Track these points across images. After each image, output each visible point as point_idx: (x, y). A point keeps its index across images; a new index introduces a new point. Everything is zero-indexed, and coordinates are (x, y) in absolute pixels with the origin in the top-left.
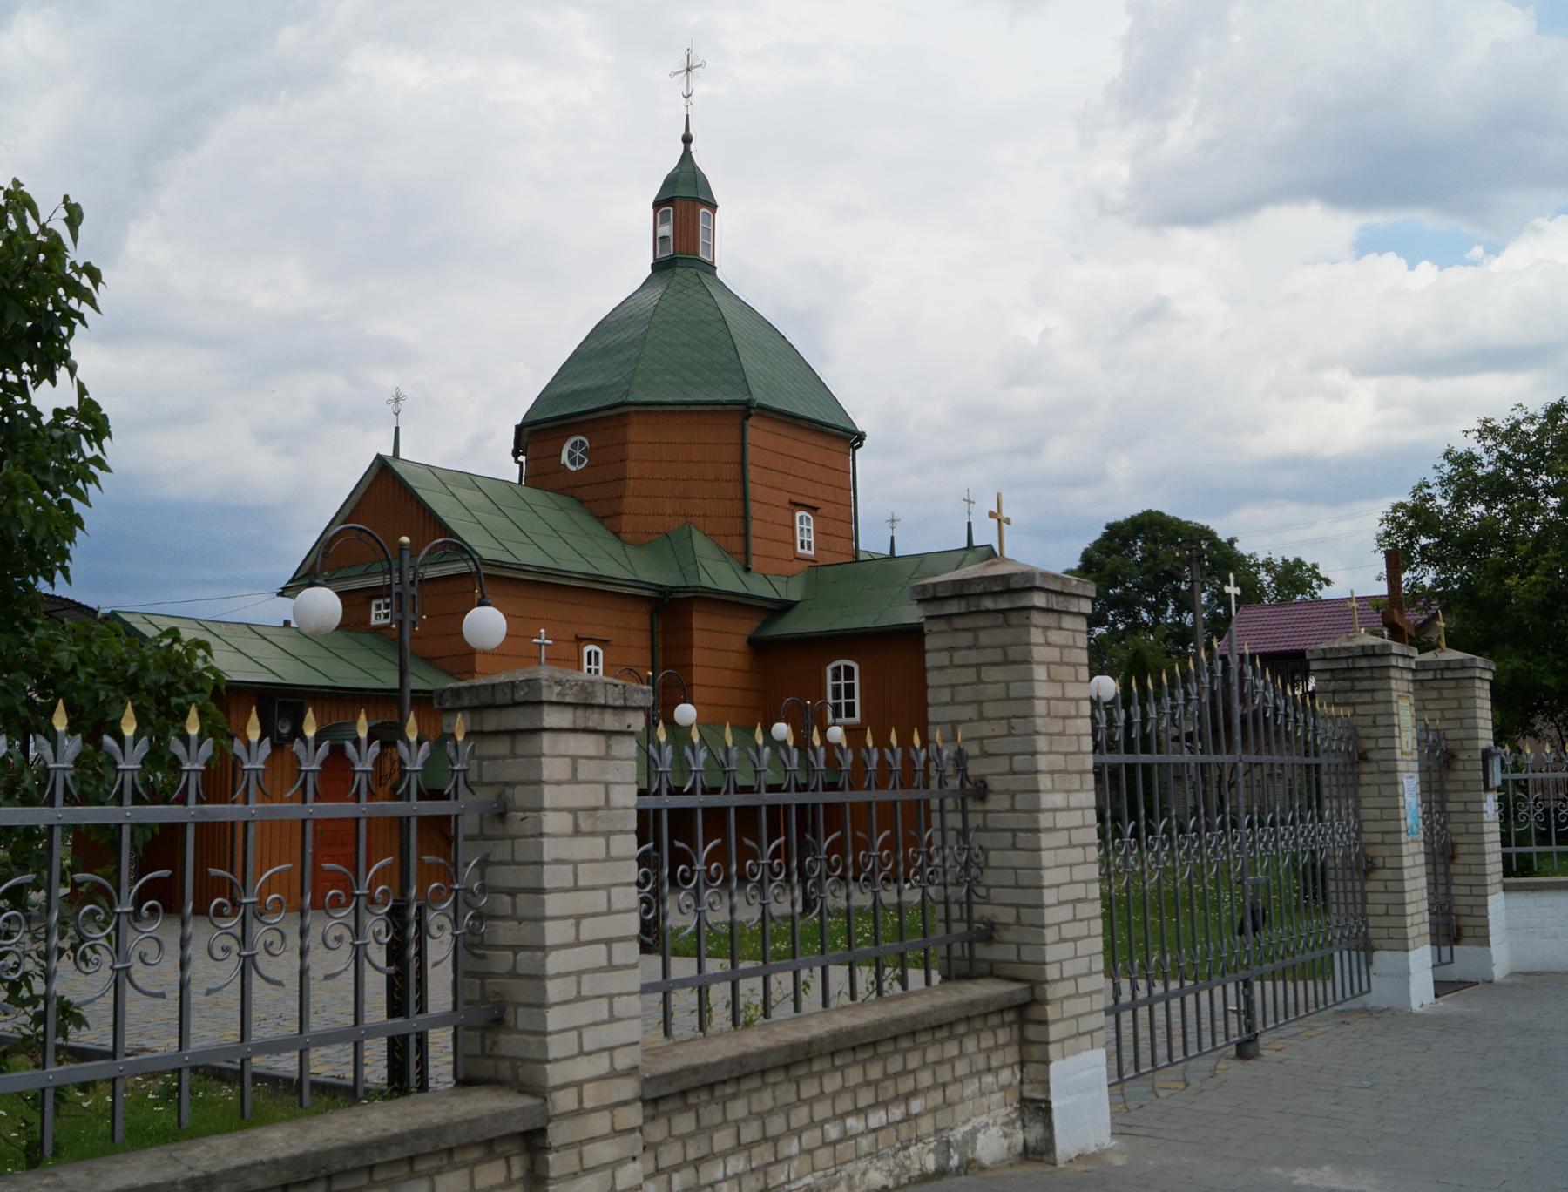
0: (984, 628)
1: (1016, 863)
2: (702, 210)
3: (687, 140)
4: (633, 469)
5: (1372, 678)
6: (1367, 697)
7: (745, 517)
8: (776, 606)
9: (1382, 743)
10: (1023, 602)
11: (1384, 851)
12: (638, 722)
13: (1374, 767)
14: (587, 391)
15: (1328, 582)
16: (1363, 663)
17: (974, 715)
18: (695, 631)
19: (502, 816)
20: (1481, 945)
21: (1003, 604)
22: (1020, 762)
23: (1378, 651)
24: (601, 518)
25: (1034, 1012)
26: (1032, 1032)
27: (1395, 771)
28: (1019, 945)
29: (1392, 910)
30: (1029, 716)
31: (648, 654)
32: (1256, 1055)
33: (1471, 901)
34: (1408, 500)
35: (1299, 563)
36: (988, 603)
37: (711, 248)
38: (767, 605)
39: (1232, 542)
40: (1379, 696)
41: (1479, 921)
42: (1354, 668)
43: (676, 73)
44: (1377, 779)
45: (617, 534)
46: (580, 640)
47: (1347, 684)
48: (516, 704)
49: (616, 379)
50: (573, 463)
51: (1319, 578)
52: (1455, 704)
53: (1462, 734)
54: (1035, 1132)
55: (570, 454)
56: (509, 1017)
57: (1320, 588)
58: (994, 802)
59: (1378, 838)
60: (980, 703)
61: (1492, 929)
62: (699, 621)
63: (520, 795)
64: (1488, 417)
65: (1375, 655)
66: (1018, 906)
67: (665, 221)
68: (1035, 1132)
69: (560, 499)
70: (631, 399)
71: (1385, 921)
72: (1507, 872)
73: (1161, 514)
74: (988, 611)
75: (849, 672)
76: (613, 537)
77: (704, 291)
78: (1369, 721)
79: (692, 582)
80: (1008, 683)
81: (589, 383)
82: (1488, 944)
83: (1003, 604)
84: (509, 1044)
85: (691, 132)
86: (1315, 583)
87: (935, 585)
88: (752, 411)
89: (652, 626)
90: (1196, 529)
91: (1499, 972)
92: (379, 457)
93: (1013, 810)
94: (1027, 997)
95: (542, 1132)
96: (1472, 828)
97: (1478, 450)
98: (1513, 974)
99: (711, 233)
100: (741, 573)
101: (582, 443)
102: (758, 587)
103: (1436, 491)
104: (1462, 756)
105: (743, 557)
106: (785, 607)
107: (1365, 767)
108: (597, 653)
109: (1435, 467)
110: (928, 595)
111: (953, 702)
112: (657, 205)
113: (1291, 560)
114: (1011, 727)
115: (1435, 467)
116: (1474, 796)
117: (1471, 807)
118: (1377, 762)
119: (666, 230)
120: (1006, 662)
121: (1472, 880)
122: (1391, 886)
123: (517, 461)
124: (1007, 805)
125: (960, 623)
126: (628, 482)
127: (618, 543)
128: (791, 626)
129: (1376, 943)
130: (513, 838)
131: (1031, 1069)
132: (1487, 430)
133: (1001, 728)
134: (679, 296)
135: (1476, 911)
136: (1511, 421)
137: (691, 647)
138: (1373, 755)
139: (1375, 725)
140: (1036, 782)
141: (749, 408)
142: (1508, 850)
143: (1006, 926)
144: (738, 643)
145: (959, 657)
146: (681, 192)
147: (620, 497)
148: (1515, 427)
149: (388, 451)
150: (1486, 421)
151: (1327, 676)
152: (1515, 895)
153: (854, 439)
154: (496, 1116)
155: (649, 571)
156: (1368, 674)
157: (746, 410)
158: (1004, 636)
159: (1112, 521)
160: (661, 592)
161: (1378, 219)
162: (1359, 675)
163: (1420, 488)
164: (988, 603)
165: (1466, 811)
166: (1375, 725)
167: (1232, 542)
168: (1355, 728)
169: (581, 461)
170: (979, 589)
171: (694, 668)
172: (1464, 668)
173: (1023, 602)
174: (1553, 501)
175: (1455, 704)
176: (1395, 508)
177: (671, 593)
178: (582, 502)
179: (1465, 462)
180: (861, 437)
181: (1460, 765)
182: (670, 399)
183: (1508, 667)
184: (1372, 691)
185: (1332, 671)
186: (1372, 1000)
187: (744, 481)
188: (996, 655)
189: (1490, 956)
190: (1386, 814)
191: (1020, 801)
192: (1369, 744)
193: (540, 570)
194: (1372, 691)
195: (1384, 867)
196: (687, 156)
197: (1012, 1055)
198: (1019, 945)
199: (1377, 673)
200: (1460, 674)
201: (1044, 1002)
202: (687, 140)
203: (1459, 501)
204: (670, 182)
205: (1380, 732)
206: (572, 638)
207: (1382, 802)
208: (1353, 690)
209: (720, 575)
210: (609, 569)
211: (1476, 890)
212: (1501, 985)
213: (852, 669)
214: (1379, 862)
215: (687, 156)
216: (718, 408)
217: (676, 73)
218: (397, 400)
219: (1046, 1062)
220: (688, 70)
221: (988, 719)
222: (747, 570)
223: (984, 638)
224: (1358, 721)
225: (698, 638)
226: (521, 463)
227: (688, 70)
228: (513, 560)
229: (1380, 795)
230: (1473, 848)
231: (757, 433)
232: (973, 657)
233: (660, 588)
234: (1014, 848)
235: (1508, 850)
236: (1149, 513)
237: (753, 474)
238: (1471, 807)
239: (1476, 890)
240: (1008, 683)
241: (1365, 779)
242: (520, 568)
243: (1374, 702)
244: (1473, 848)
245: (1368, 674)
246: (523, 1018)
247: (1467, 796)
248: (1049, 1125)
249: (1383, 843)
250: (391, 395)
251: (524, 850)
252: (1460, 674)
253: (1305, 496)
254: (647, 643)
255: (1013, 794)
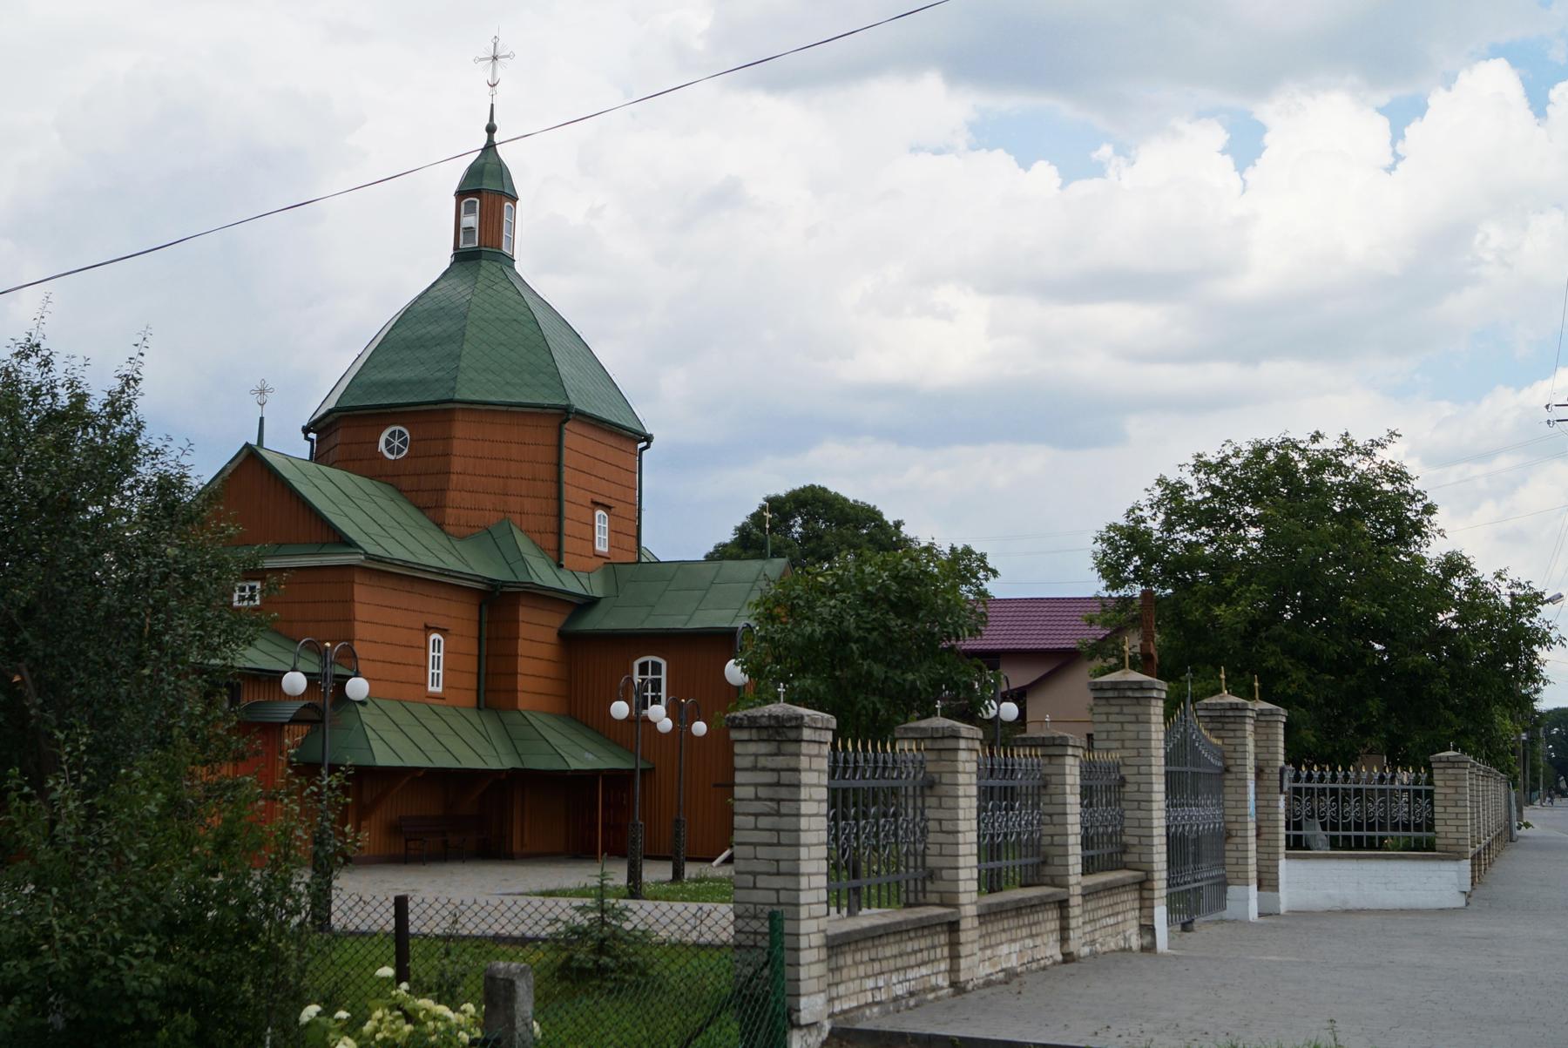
0: (1126, 705)
1: (1139, 816)
2: (507, 204)
3: (491, 129)
4: (457, 464)
5: (1235, 723)
6: (1231, 734)
7: (559, 516)
8: (579, 601)
9: (1239, 762)
10: (1148, 694)
11: (1237, 826)
12: (829, 736)
13: (1232, 776)
14: (408, 382)
15: (995, 573)
16: (1230, 713)
17: (1120, 746)
18: (521, 625)
19: (1045, 787)
20: (1272, 891)
21: (1138, 694)
22: (1143, 769)
23: (1240, 707)
24: (422, 509)
25: (1147, 885)
26: (1146, 894)
27: (1246, 779)
28: (1140, 854)
29: (1240, 861)
30: (1149, 748)
31: (475, 642)
32: (1191, 930)
33: (1268, 863)
34: (1122, 522)
35: (968, 551)
36: (1130, 693)
37: (512, 241)
38: (575, 600)
39: (898, 524)
40: (1239, 734)
41: (1273, 876)
42: (1224, 716)
43: (481, 59)
44: (1236, 783)
45: (440, 525)
46: (428, 629)
47: (1220, 725)
48: (1054, 745)
49: (439, 374)
50: (391, 451)
51: (986, 568)
52: (1265, 737)
53: (1268, 756)
54: (1147, 939)
55: (388, 443)
56: (1050, 861)
57: (987, 579)
58: (1128, 788)
59: (1233, 819)
60: (1123, 740)
61: (1280, 881)
62: (524, 613)
63: (1054, 779)
64: (1201, 453)
65: (1237, 709)
66: (1140, 836)
67: (470, 211)
68: (1147, 939)
69: (383, 487)
70: (457, 397)
71: (1236, 868)
72: (1288, 847)
73: (825, 490)
74: (1129, 697)
75: (657, 668)
76: (436, 528)
77: (512, 288)
78: (1232, 748)
79: (523, 578)
80: (1138, 732)
81: (408, 374)
82: (1277, 891)
83: (1138, 694)
84: (1048, 870)
85: (496, 122)
86: (981, 574)
87: (1102, 682)
88: (571, 416)
89: (480, 616)
90: (863, 509)
91: (1283, 909)
92: (247, 445)
93: (1138, 791)
94: (1145, 878)
95: (1067, 900)
96: (1271, 817)
97: (1191, 481)
98: (1289, 911)
99: (513, 225)
100: (555, 569)
101: (401, 434)
102: (572, 586)
103: (1147, 513)
104: (1268, 770)
105: (554, 554)
106: (589, 603)
107: (1229, 776)
108: (439, 641)
109: (1146, 490)
110: (1098, 687)
111: (1108, 739)
112: (461, 194)
113: (960, 547)
114: (1139, 753)
115: (1146, 490)
116: (1273, 796)
117: (1271, 803)
118: (1236, 773)
119: (471, 221)
120: (1138, 722)
121: (1270, 850)
122: (1240, 847)
123: (307, 438)
124: (1136, 789)
125: (1113, 702)
126: (452, 476)
127: (442, 538)
128: (597, 621)
129: (1229, 881)
130: (1051, 795)
131: (1145, 912)
132: (1201, 465)
133: (1134, 753)
134: (489, 291)
135: (1271, 870)
136: (1222, 455)
137: (517, 638)
138: (1234, 769)
139: (1235, 751)
140: (1151, 779)
141: (569, 413)
142: (1288, 833)
143: (1134, 845)
144: (552, 636)
145: (1112, 718)
146: (488, 184)
147: (443, 490)
148: (1224, 462)
149: (254, 442)
150: (1200, 456)
151: (1207, 720)
152: (1292, 861)
153: (637, 438)
154: (938, 916)
155: (479, 565)
156: (1232, 720)
157: (565, 414)
158: (1138, 709)
159: (772, 493)
160: (492, 586)
161: (1011, 103)
162: (1227, 720)
163: (1132, 510)
164: (1130, 693)
165: (1268, 806)
166: (1235, 751)
167: (898, 524)
168: (1223, 752)
169: (400, 451)
170: (1126, 687)
171: (519, 659)
172: (1272, 714)
173: (1148, 694)
174: (1253, 532)
175: (1265, 737)
176: (1109, 528)
177: (502, 587)
178: (400, 491)
179: (1174, 492)
180: (648, 439)
181: (1265, 777)
182: (493, 399)
183: (1209, 687)
184: (1234, 730)
185: (1210, 717)
186: (1226, 914)
187: (559, 481)
188: (1133, 718)
189: (1279, 898)
190: (1240, 804)
191: (1143, 787)
192: (1231, 762)
193: (406, 564)
194: (1234, 730)
195: (1236, 836)
196: (490, 146)
197: (1137, 905)
198: (1140, 854)
199: (1238, 720)
200: (1269, 718)
201: (1152, 880)
202: (491, 129)
203: (1169, 526)
204: (474, 172)
205: (1238, 755)
206: (422, 627)
207: (1238, 797)
208: (1223, 729)
209: (543, 574)
210: (452, 563)
211: (1272, 856)
212: (1283, 916)
213: (660, 665)
214: (1234, 833)
215: (490, 146)
216: (539, 410)
217: (481, 59)
218: (262, 392)
219: (1153, 907)
220: (495, 58)
221: (1127, 749)
222: (561, 566)
223: (1125, 710)
224: (1225, 748)
225: (524, 630)
226: (311, 440)
227: (495, 58)
228: (387, 555)
229: (1236, 793)
230: (1271, 830)
231: (573, 437)
232: (1120, 718)
233: (492, 583)
234: (1139, 809)
235: (1288, 833)
236: (812, 488)
237: (567, 475)
238: (1271, 803)
239: (1272, 856)
240: (1138, 732)
241: (1228, 783)
242: (392, 562)
243: (1235, 737)
244: (1271, 830)
245: (1232, 720)
246: (1057, 861)
247: (1269, 797)
248: (1154, 936)
249: (1236, 822)
250: (256, 384)
251: (1056, 799)
252: (1269, 718)
253: (899, 435)
254: (475, 633)
255: (1139, 784)
